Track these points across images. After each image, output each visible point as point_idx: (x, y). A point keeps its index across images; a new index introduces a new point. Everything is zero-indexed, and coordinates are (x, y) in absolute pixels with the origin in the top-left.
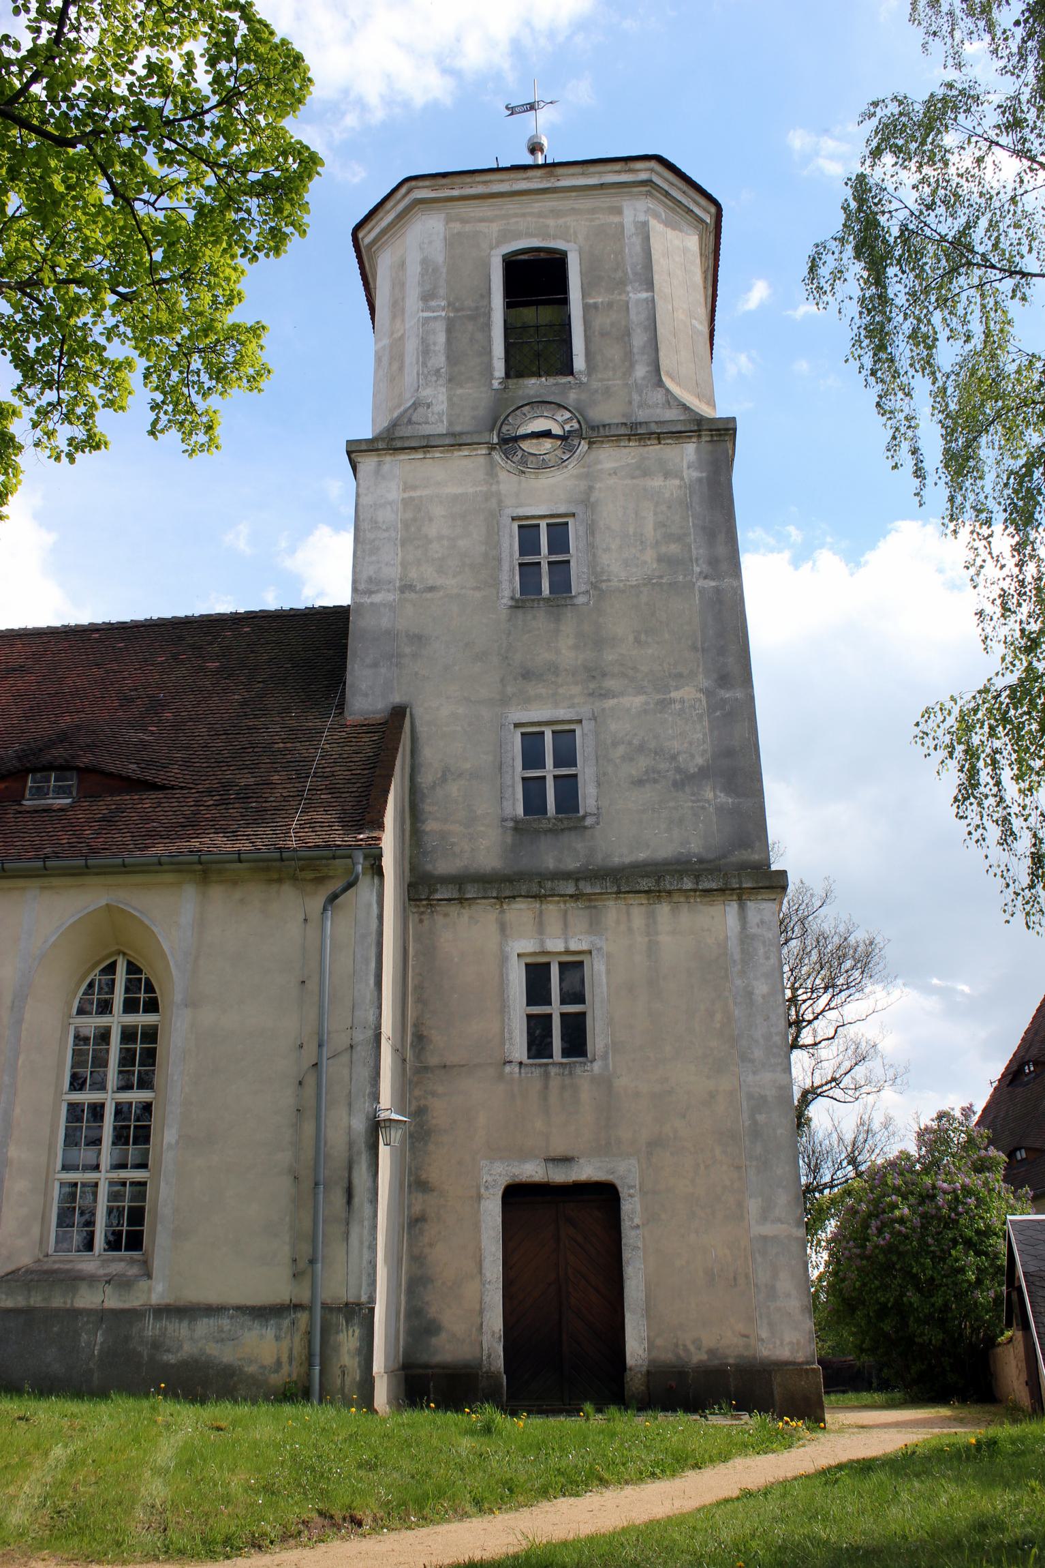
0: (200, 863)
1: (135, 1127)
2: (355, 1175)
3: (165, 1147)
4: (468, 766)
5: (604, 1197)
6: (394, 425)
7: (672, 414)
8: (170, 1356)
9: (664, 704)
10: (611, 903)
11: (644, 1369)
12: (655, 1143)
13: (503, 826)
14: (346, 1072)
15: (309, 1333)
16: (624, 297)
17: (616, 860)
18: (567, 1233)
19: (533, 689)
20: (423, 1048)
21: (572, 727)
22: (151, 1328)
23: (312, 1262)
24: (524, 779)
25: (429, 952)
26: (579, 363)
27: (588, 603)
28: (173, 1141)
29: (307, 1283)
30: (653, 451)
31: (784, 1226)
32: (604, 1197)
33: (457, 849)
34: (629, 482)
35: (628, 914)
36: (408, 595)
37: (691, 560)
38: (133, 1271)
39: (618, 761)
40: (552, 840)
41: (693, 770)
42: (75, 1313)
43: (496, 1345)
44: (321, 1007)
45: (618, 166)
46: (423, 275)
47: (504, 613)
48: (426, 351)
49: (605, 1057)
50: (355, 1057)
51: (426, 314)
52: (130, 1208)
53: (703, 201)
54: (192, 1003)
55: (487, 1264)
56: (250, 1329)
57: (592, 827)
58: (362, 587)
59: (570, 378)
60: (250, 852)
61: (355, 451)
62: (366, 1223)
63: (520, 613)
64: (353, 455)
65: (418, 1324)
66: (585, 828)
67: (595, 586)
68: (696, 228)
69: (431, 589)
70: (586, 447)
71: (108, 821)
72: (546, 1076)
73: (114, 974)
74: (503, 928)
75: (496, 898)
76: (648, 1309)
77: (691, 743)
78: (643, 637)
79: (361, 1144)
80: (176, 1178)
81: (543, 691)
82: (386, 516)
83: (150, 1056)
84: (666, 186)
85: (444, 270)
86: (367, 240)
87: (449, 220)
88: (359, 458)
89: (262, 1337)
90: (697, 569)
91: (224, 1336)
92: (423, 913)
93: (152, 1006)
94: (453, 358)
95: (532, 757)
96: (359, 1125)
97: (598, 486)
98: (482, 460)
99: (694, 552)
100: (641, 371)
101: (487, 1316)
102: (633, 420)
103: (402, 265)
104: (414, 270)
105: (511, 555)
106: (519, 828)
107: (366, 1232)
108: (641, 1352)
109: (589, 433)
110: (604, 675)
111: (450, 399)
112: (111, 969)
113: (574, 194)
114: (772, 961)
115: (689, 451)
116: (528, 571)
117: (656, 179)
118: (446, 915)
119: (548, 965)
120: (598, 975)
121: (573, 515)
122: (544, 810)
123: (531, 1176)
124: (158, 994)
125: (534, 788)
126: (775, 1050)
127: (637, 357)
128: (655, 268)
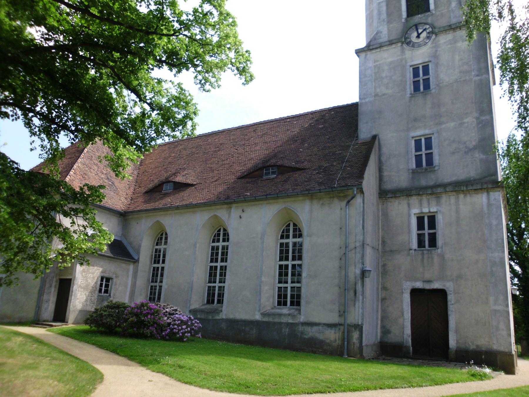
2: (357, 287)
5: (442, 294)
6: (370, 42)
9: (461, 124)
10: (444, 195)
11: (455, 349)
14: (354, 255)
15: (344, 332)
18: (430, 304)
21: (431, 136)
22: (301, 328)
23: (344, 312)
24: (416, 156)
25: (386, 215)
26: (432, 6)
32: (442, 294)
36: (377, 98)
38: (296, 313)
41: (471, 147)
42: (280, 323)
48: (379, 14)
49: (442, 248)
54: (309, 236)
55: (405, 313)
57: (437, 170)
59: (429, 13)
63: (413, 99)
66: (435, 170)
67: (438, 85)
69: (384, 95)
71: (286, 181)
72: (423, 254)
74: (409, 205)
79: (359, 277)
80: (308, 287)
83: (300, 251)
89: (331, 332)
90: (473, 73)
93: (300, 236)
94: (389, 14)
95: (418, 147)
96: (358, 272)
97: (439, 50)
101: (405, 329)
105: (410, 79)
106: (414, 172)
109: (434, 32)
110: (441, 116)
111: (388, 29)
112: (289, 225)
116: (416, 84)
118: (391, 202)
120: (440, 219)
121: (430, 61)
122: (422, 165)
125: (418, 158)
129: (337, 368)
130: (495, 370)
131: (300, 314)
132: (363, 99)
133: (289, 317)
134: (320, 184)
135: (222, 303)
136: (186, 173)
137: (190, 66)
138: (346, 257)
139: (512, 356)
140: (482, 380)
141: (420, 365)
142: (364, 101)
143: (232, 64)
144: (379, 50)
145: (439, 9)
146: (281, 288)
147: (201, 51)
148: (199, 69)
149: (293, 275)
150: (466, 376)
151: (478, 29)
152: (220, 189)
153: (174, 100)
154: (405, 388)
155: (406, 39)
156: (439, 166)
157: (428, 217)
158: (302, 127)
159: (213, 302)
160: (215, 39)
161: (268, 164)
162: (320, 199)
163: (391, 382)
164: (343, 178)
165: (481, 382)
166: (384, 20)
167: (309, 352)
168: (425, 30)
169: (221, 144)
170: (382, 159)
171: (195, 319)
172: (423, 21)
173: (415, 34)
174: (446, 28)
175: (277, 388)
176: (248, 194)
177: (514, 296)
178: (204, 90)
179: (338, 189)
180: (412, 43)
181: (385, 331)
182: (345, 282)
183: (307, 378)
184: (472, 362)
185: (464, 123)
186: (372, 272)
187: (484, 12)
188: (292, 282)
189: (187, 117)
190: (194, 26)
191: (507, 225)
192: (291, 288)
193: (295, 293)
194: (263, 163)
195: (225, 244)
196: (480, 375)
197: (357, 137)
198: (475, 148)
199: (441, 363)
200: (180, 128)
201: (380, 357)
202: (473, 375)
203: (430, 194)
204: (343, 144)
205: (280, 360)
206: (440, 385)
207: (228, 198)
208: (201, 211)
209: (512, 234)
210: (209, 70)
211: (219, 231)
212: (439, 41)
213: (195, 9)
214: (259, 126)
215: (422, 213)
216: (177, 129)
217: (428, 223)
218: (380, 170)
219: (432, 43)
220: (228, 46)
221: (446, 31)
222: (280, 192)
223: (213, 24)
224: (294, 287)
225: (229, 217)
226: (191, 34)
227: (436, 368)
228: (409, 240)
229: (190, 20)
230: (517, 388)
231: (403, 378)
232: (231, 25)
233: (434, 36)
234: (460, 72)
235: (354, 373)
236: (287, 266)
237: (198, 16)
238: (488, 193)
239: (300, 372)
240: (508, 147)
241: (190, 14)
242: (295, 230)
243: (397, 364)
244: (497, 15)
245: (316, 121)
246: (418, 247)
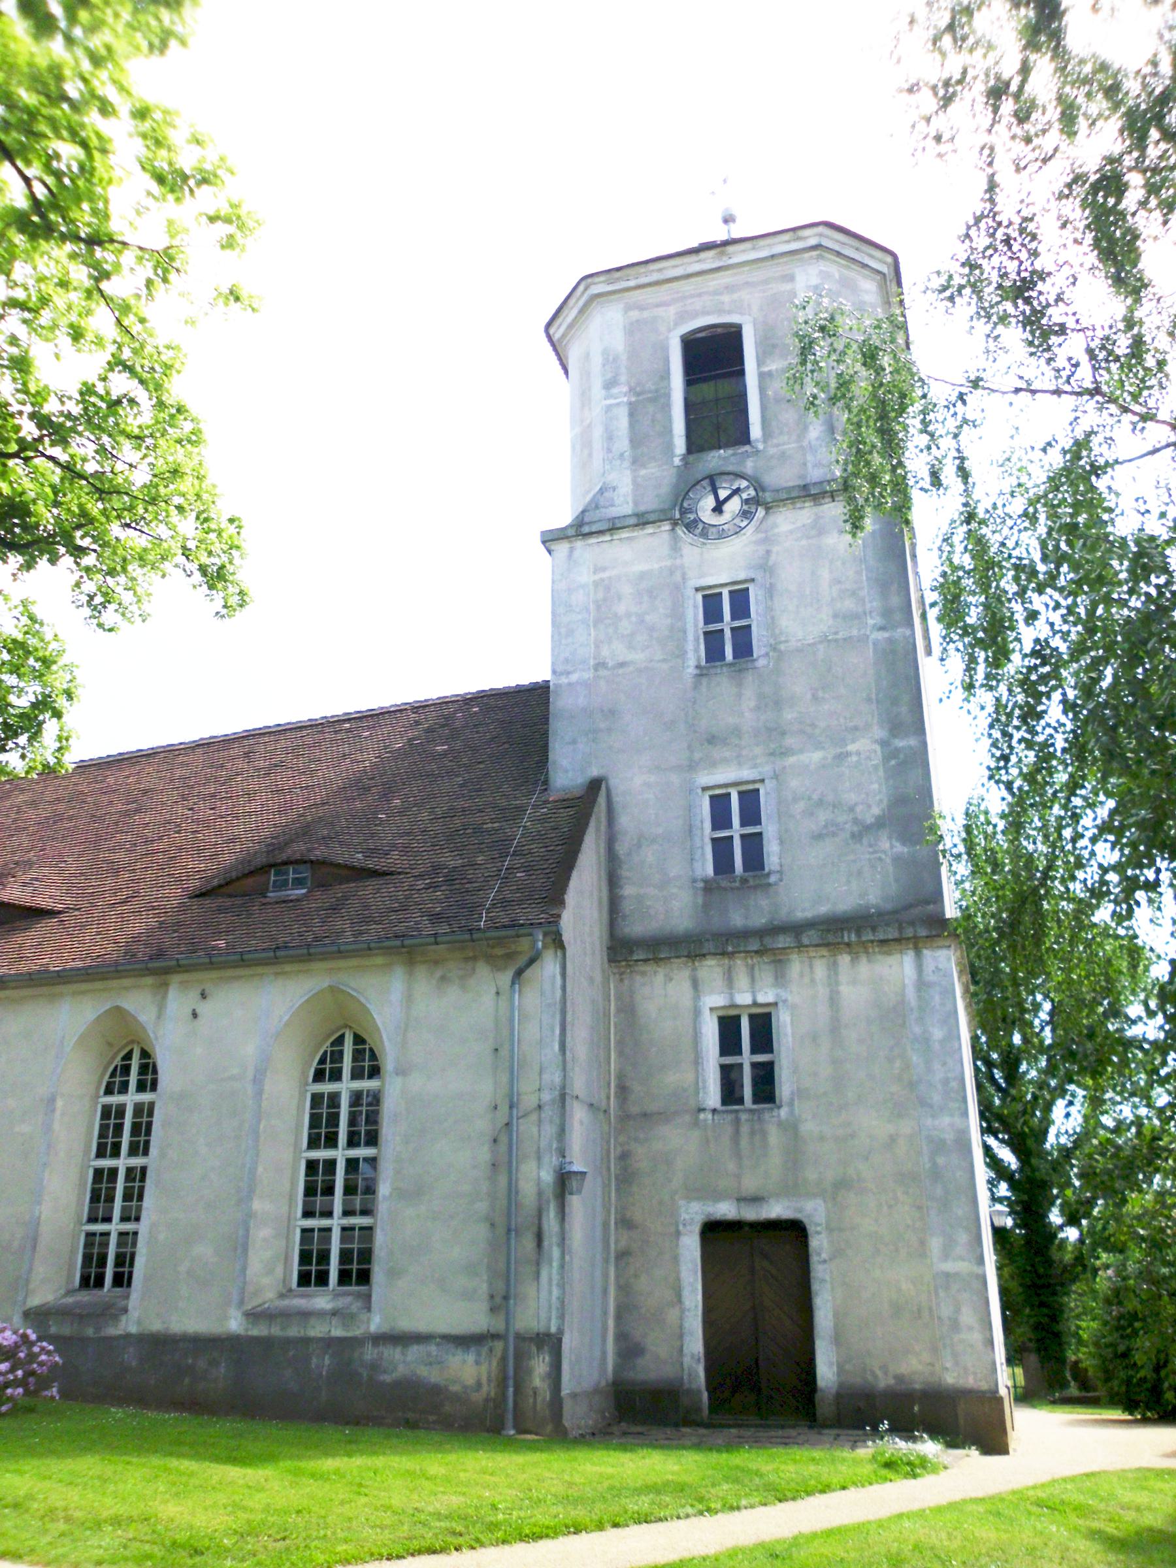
4: (660, 830)
6: (583, 512)
9: (841, 757)
11: (834, 1391)
14: (535, 1130)
15: (504, 1359)
18: (761, 1260)
19: (717, 752)
21: (756, 786)
22: (370, 1353)
23: (506, 1298)
25: (628, 1010)
26: (756, 431)
29: (502, 1316)
31: (966, 1264)
33: (652, 912)
34: (804, 542)
35: (811, 967)
36: (603, 672)
38: (356, 1306)
41: (870, 820)
42: (307, 1341)
44: (512, 1073)
45: (786, 237)
48: (610, 438)
49: (791, 1104)
51: (609, 402)
54: (401, 1072)
55: (686, 1293)
57: (776, 884)
59: (747, 448)
62: (555, 1264)
63: (704, 681)
66: (769, 885)
67: (774, 648)
69: (622, 665)
72: (737, 1122)
74: (695, 984)
78: (820, 694)
79: (549, 1193)
80: (394, 1226)
83: (373, 1118)
84: (837, 247)
85: (624, 357)
87: (628, 308)
90: (871, 622)
93: (375, 1072)
94: (636, 441)
95: (720, 818)
96: (547, 1176)
97: (775, 549)
99: (868, 606)
101: (687, 1339)
103: (587, 356)
104: (597, 360)
105: (696, 626)
106: (709, 887)
107: (554, 1271)
109: (762, 500)
110: (783, 733)
112: (340, 1040)
116: (713, 642)
117: (825, 242)
118: (643, 974)
119: (738, 1017)
120: (785, 1026)
125: (722, 848)
129: (484, 1472)
130: (951, 1445)
131: (369, 1309)
132: (561, 674)
134: (436, 918)
135: (129, 1284)
136: (35, 875)
137: (62, 550)
138: (510, 1136)
139: (1000, 1400)
140: (915, 1476)
141: (730, 1446)
142: (564, 680)
143: (186, 552)
144: (607, 538)
146: (312, 1230)
147: (95, 508)
148: (89, 560)
149: (349, 1190)
150: (867, 1469)
151: (879, 506)
152: (138, 926)
153: (9, 651)
154: (687, 1516)
155: (684, 512)
156: (780, 872)
157: (752, 1017)
158: (386, 747)
159: (99, 1282)
160: (141, 478)
161: (284, 857)
162: (436, 962)
163: (644, 1503)
164: (504, 903)
165: (913, 1482)
166: (622, 455)
167: (396, 1424)
168: (737, 492)
169: (145, 792)
171: (40, 1339)
172: (730, 468)
173: (709, 502)
175: (287, 1549)
176: (222, 943)
177: (999, 1233)
178: (100, 625)
179: (488, 934)
180: (700, 526)
181: (629, 1350)
182: (509, 1203)
183: (386, 1508)
184: (885, 1425)
185: (848, 754)
186: (589, 1177)
187: (894, 469)
188: (347, 1213)
189: (43, 704)
190: (80, 434)
191: (975, 1039)
192: (344, 1229)
193: (355, 1246)
194: (268, 852)
195: (146, 1097)
196: (909, 1463)
197: (546, 782)
198: (879, 823)
199: (793, 1432)
200: (23, 740)
201: (615, 1429)
202: (889, 1465)
203: (756, 952)
204: (503, 803)
205: (300, 1458)
206: (794, 1499)
207: (160, 954)
208: (74, 994)
209: (989, 1064)
210: (119, 568)
211: (128, 1056)
212: (775, 525)
213: (85, 384)
214: (262, 740)
216: (10, 745)
217: (749, 1036)
218: (613, 881)
219: (757, 530)
220: (177, 500)
221: (793, 499)
222: (316, 939)
223: (136, 431)
224: (352, 1229)
225: (161, 1008)
226: (72, 457)
227: (781, 1450)
229: (69, 416)
230: (1014, 1492)
231: (681, 1489)
232: (189, 441)
233: (761, 512)
234: (835, 616)
235: (533, 1483)
236: (331, 1164)
237: (94, 405)
238: (918, 951)
239: (363, 1490)
240: (968, 829)
241: (70, 398)
242: (358, 1055)
243: (662, 1447)
244: (928, 479)
245: (429, 730)
246: (725, 1102)
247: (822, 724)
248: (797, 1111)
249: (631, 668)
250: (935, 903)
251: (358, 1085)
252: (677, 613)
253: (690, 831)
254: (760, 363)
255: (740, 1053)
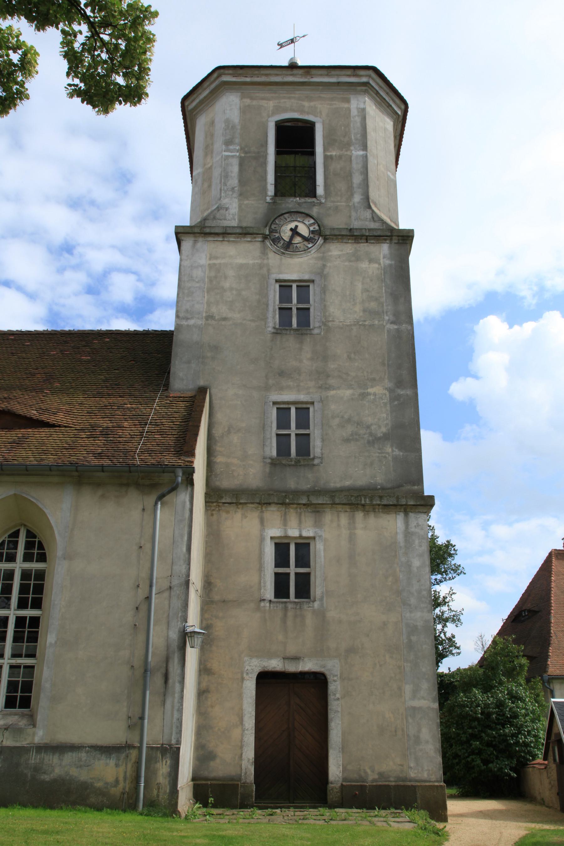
0: (77, 471)
1: (28, 632)
3: (48, 644)
4: (244, 425)
5: (318, 682)
6: (205, 219)
7: (373, 225)
8: (46, 776)
9: (364, 396)
12: (351, 651)
13: (264, 462)
16: (348, 153)
17: (332, 485)
18: (294, 703)
20: (211, 590)
21: (308, 406)
22: (33, 759)
26: (320, 190)
27: (320, 334)
28: (53, 642)
29: (137, 733)
30: (364, 247)
32: (318, 682)
34: (347, 263)
36: (210, 322)
37: (383, 312)
38: (23, 723)
39: (335, 427)
40: (291, 476)
41: (380, 435)
43: (250, 767)
45: (349, 72)
46: (225, 130)
47: (269, 336)
48: (225, 176)
49: (321, 599)
50: (173, 593)
51: (227, 154)
52: (22, 681)
53: (398, 101)
54: (68, 557)
55: (246, 719)
56: (99, 760)
57: (318, 465)
58: (181, 315)
59: (314, 200)
60: (109, 466)
61: (181, 234)
63: (279, 337)
64: (179, 235)
65: (204, 755)
66: (314, 465)
67: (324, 324)
68: (392, 117)
69: (225, 319)
70: (322, 241)
72: (286, 609)
73: (18, 537)
74: (262, 521)
75: (259, 503)
76: (343, 748)
77: (379, 419)
78: (353, 356)
81: (291, 383)
82: (198, 273)
83: (39, 589)
85: (239, 127)
86: (190, 107)
88: (182, 237)
91: (82, 763)
92: (213, 510)
93: (42, 558)
94: (242, 182)
95: (283, 422)
96: (174, 635)
97: (329, 265)
98: (258, 245)
99: (385, 308)
100: (357, 198)
101: (245, 749)
102: (352, 227)
103: (212, 123)
104: (219, 127)
106: (274, 463)
107: (176, 700)
108: (338, 773)
109: (323, 234)
110: (328, 376)
111: (240, 206)
112: (16, 534)
113: (321, 88)
114: (423, 548)
115: (385, 248)
116: (284, 311)
118: (228, 512)
119: (288, 544)
120: (319, 551)
123: (274, 667)
124: (47, 551)
125: (283, 441)
126: (423, 599)
127: (355, 190)
128: (368, 137)
131: (34, 726)
133: (7, 734)
145: (332, 199)
157: (297, 545)
166: (233, 188)
170: (214, 431)
174: (344, 233)
188: (14, 656)
192: (12, 667)
193: (20, 679)
198: (386, 437)
212: (329, 250)
215: (287, 537)
224: (19, 667)
228: (260, 583)
238: (406, 513)
242: (29, 545)
247: (353, 374)
248: (325, 605)
249: (231, 322)
250: (418, 485)
251: (28, 565)
252: (263, 292)
253: (264, 428)
254: (325, 150)
255: (288, 566)
